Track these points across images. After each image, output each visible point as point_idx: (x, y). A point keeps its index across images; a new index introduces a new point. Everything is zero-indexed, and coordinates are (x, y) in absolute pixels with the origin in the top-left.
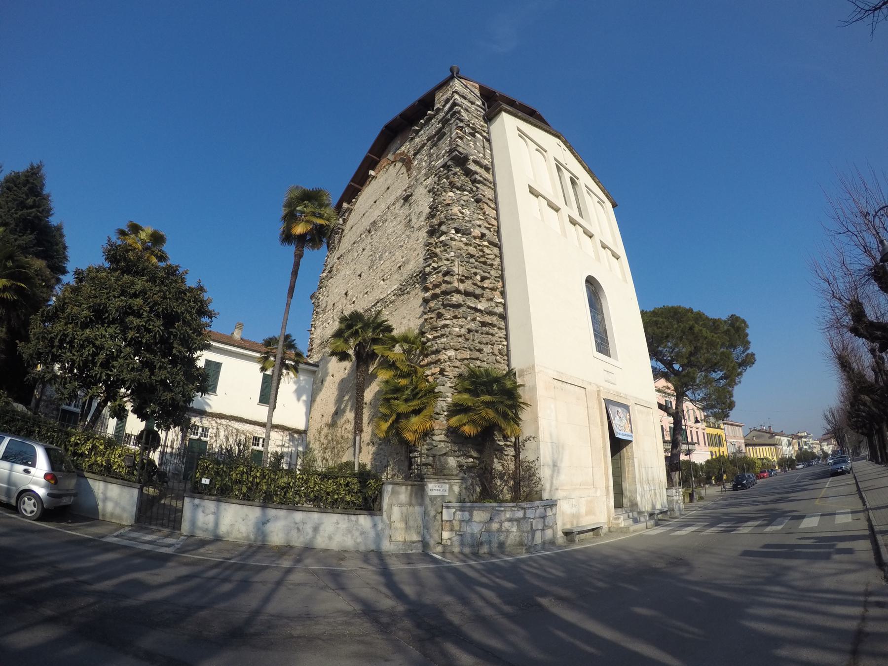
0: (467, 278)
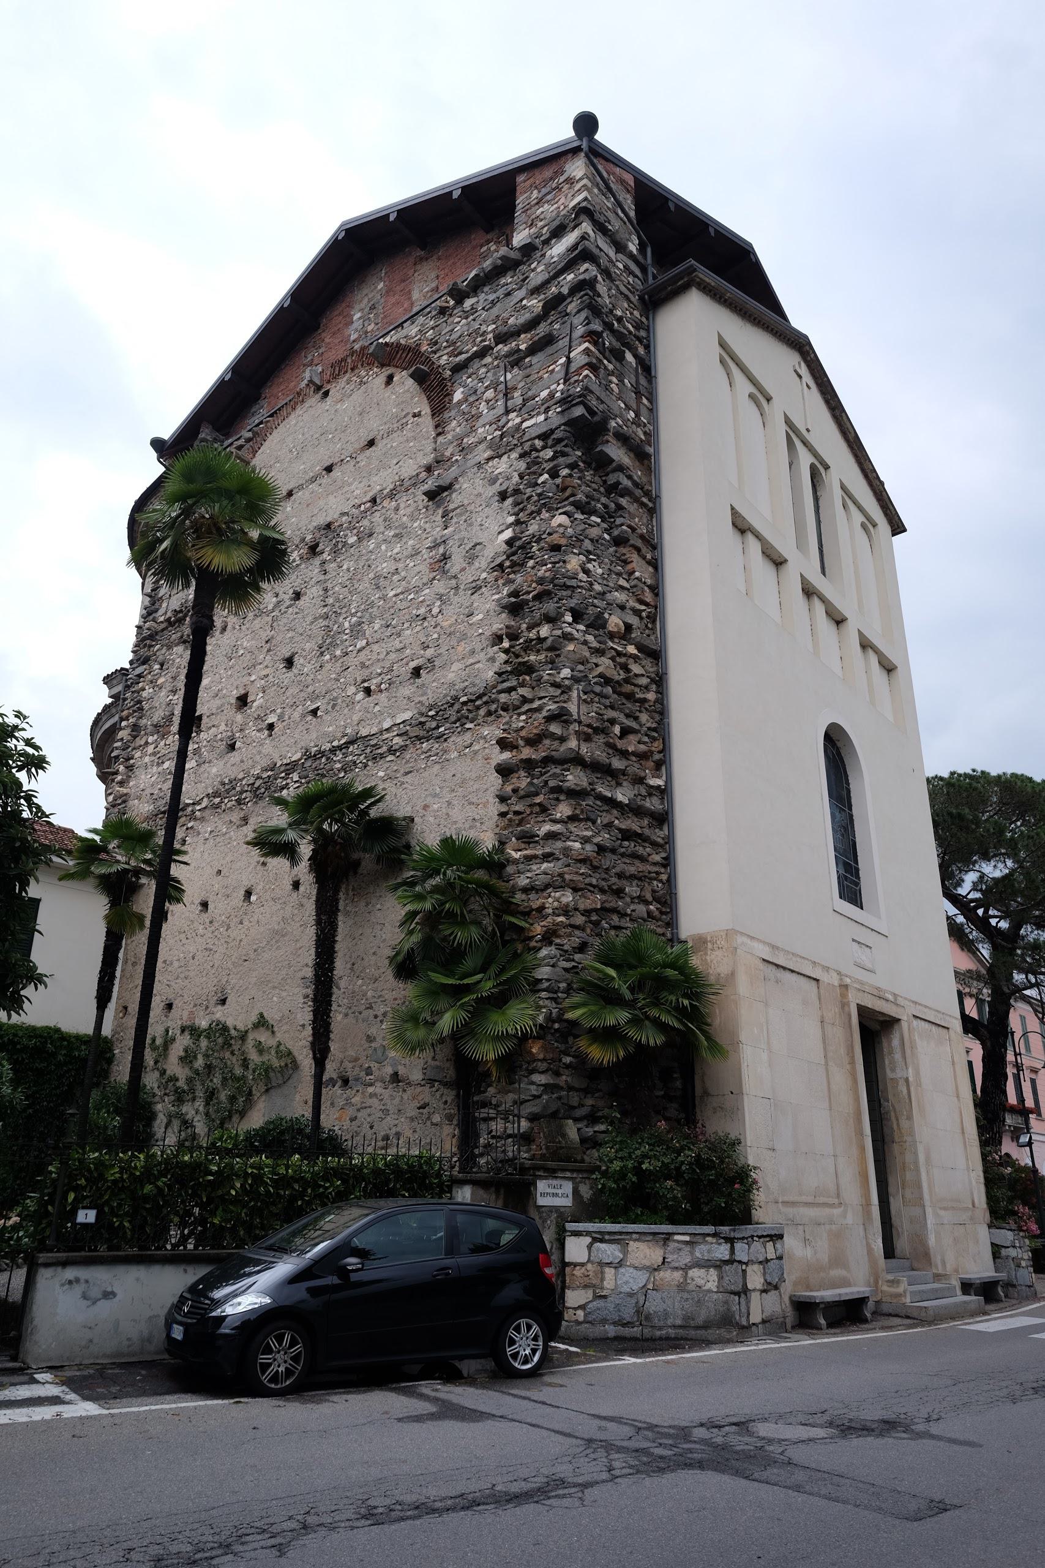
0: (597, 731)
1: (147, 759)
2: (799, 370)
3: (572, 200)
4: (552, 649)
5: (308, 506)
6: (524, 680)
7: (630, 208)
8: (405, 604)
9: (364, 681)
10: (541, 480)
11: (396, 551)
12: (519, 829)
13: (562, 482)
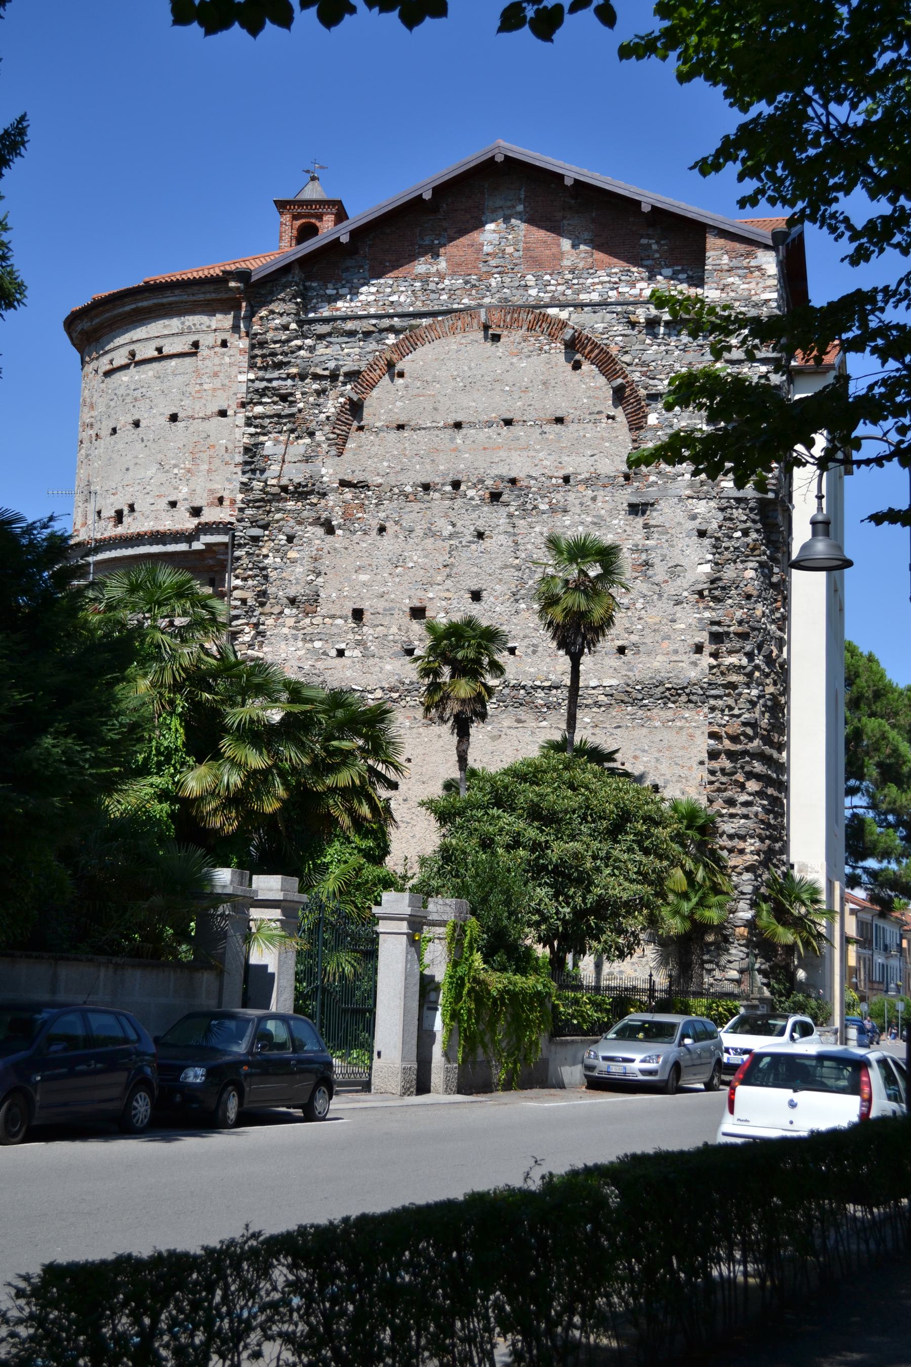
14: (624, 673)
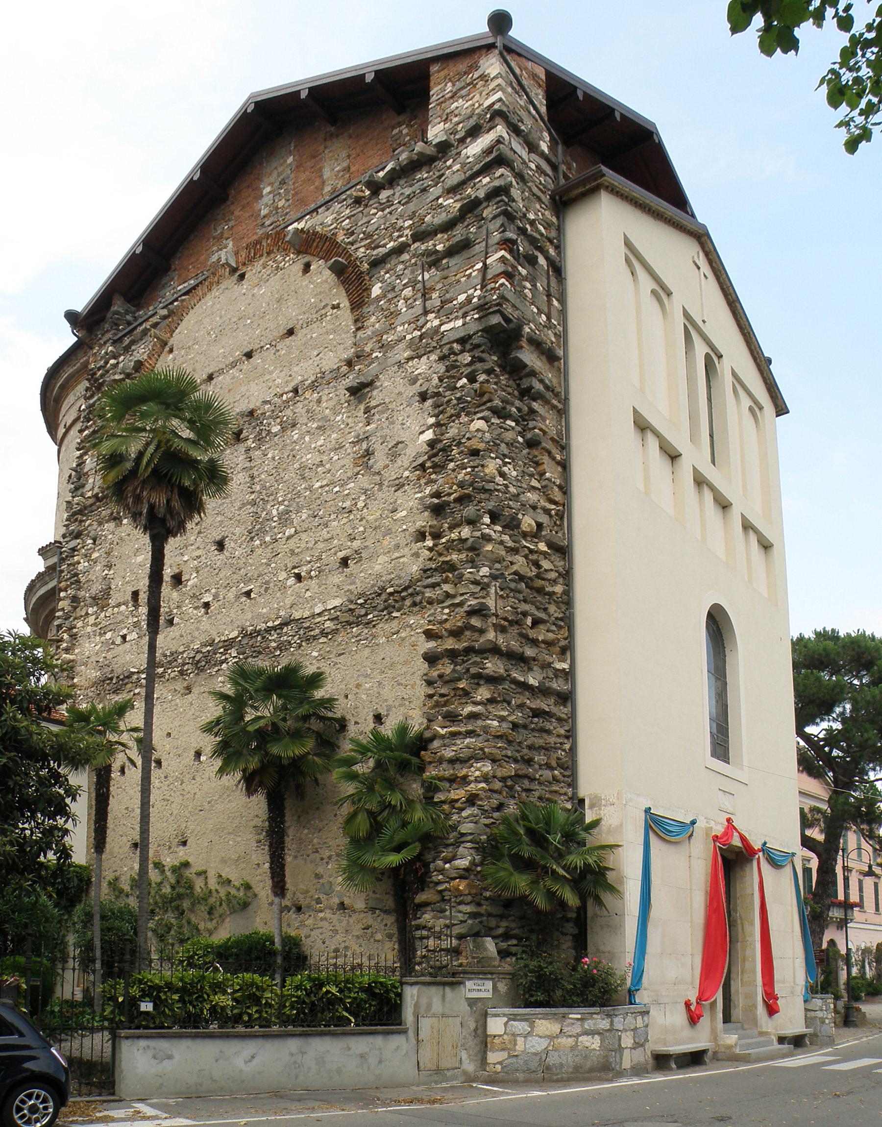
1: (89, 629)
2: (697, 261)
3: (487, 99)
4: (472, 549)
5: (229, 391)
6: (447, 577)
7: (541, 103)
8: (330, 496)
9: (294, 567)
10: (460, 383)
11: (320, 443)
12: (445, 709)
13: (481, 388)
14: (346, 588)
